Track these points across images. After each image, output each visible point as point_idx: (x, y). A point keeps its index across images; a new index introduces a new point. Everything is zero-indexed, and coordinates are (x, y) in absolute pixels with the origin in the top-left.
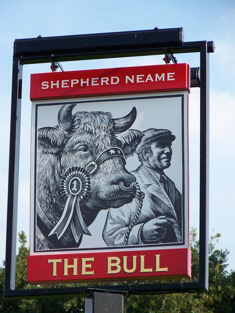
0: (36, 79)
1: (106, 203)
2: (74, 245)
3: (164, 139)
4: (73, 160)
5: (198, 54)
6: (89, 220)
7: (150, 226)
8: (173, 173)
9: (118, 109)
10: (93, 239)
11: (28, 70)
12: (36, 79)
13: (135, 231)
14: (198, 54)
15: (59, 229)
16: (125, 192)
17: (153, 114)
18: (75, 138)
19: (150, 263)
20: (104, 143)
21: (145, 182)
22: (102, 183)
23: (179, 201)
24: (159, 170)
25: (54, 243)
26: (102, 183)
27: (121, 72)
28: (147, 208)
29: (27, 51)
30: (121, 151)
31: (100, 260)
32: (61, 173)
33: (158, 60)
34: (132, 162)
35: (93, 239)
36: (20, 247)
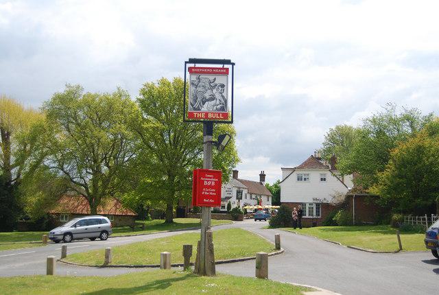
0: (189, 68)
1: (208, 100)
2: (199, 110)
3: (223, 86)
4: (199, 89)
5: (216, 266)
6: (203, 104)
7: (219, 107)
8: (224, 94)
9: (211, 77)
10: (204, 109)
11: (230, 120)
12: (189, 68)
13: (215, 108)
14: (216, 266)
15: (196, 105)
16: (212, 98)
17: (220, 80)
18: (200, 84)
19: (219, 115)
20: (208, 86)
21: (218, 96)
22: (207, 95)
23: (226, 101)
24: (221, 93)
25: (195, 109)
26: (207, 95)
27: (213, 69)
28: (218, 102)
29: (191, 61)
30: (212, 88)
31: (207, 114)
32: (197, 92)
33: (221, 66)
34: (215, 91)
35: (204, 109)
36: (93, 93)
